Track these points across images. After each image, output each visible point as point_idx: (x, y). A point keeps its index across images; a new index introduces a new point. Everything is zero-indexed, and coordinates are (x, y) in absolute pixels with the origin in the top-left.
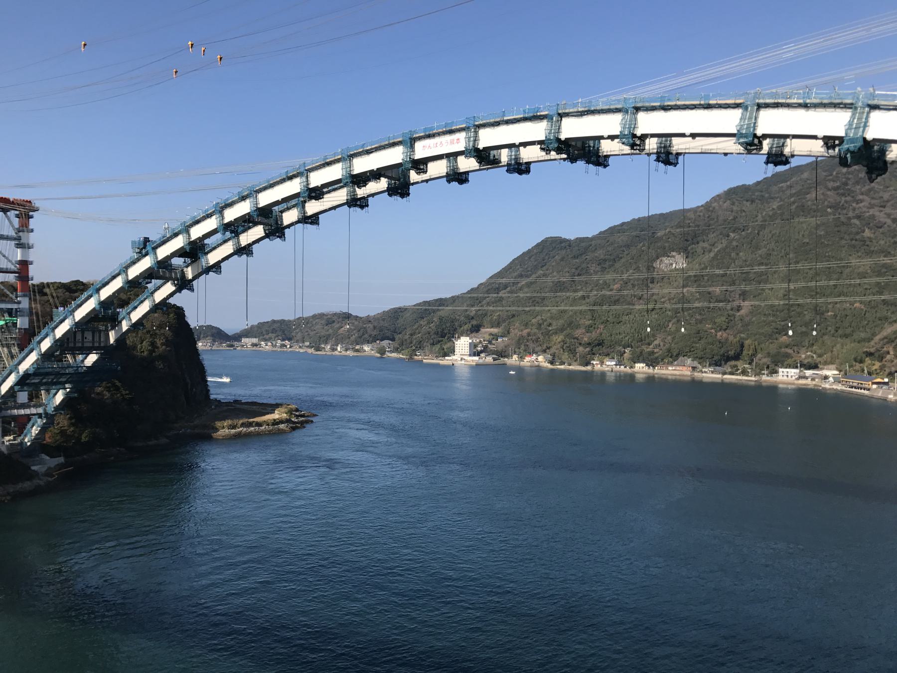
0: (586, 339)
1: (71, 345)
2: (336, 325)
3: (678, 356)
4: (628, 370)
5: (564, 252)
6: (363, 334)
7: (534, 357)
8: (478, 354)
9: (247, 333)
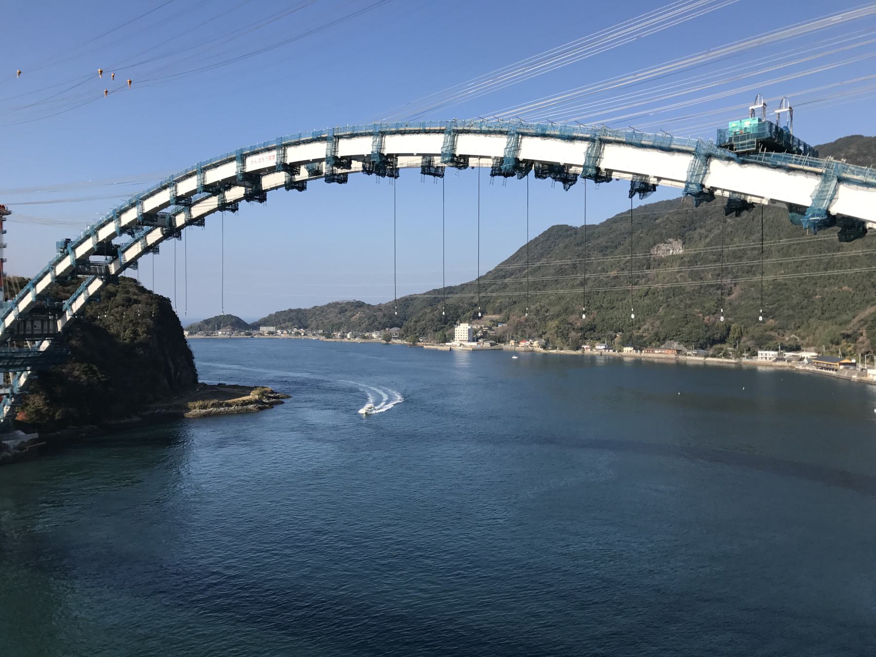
0: (579, 324)
1: (22, 333)
2: (348, 314)
3: (664, 339)
4: (616, 353)
5: (567, 240)
6: (373, 322)
7: (528, 343)
8: (476, 340)
9: (265, 322)
